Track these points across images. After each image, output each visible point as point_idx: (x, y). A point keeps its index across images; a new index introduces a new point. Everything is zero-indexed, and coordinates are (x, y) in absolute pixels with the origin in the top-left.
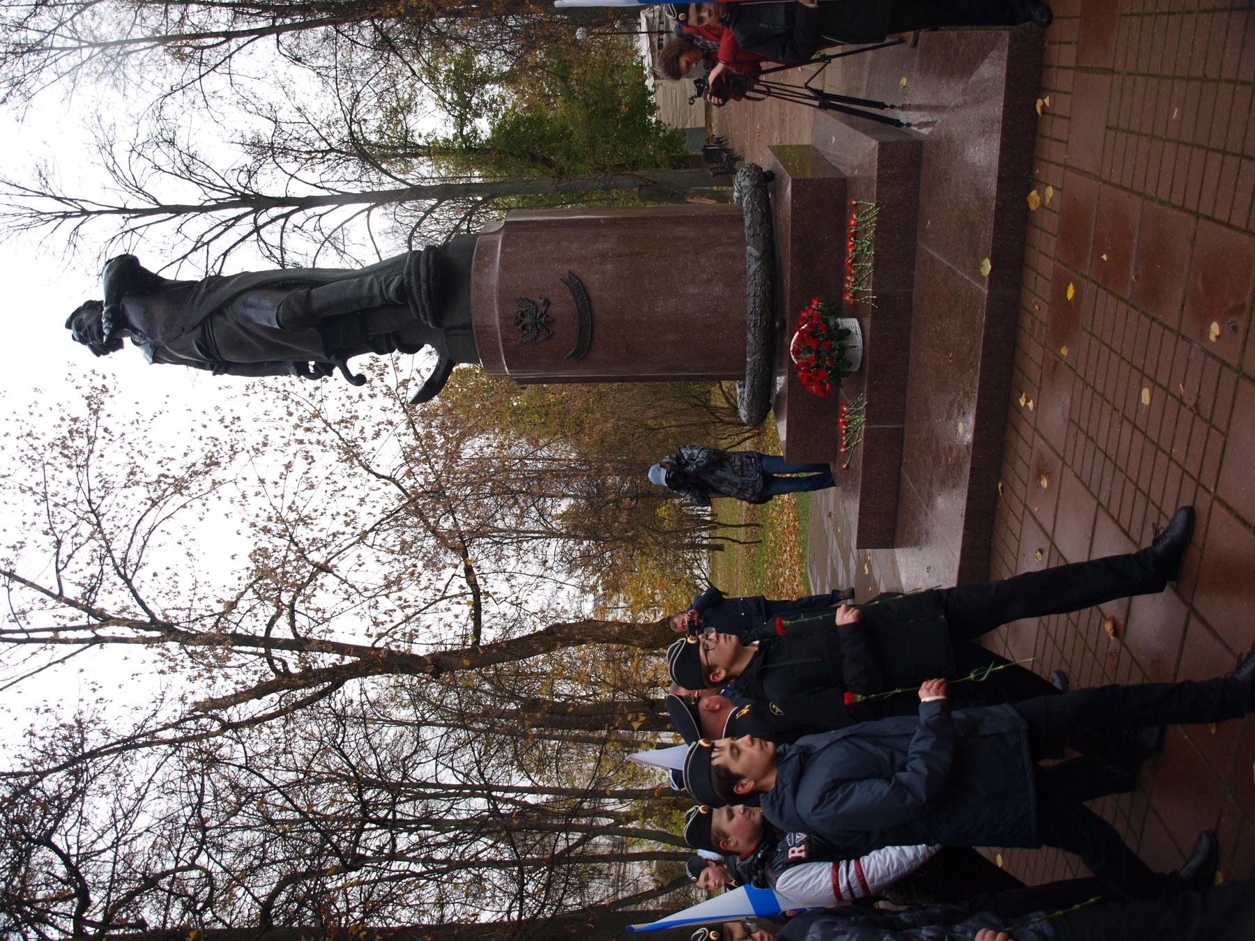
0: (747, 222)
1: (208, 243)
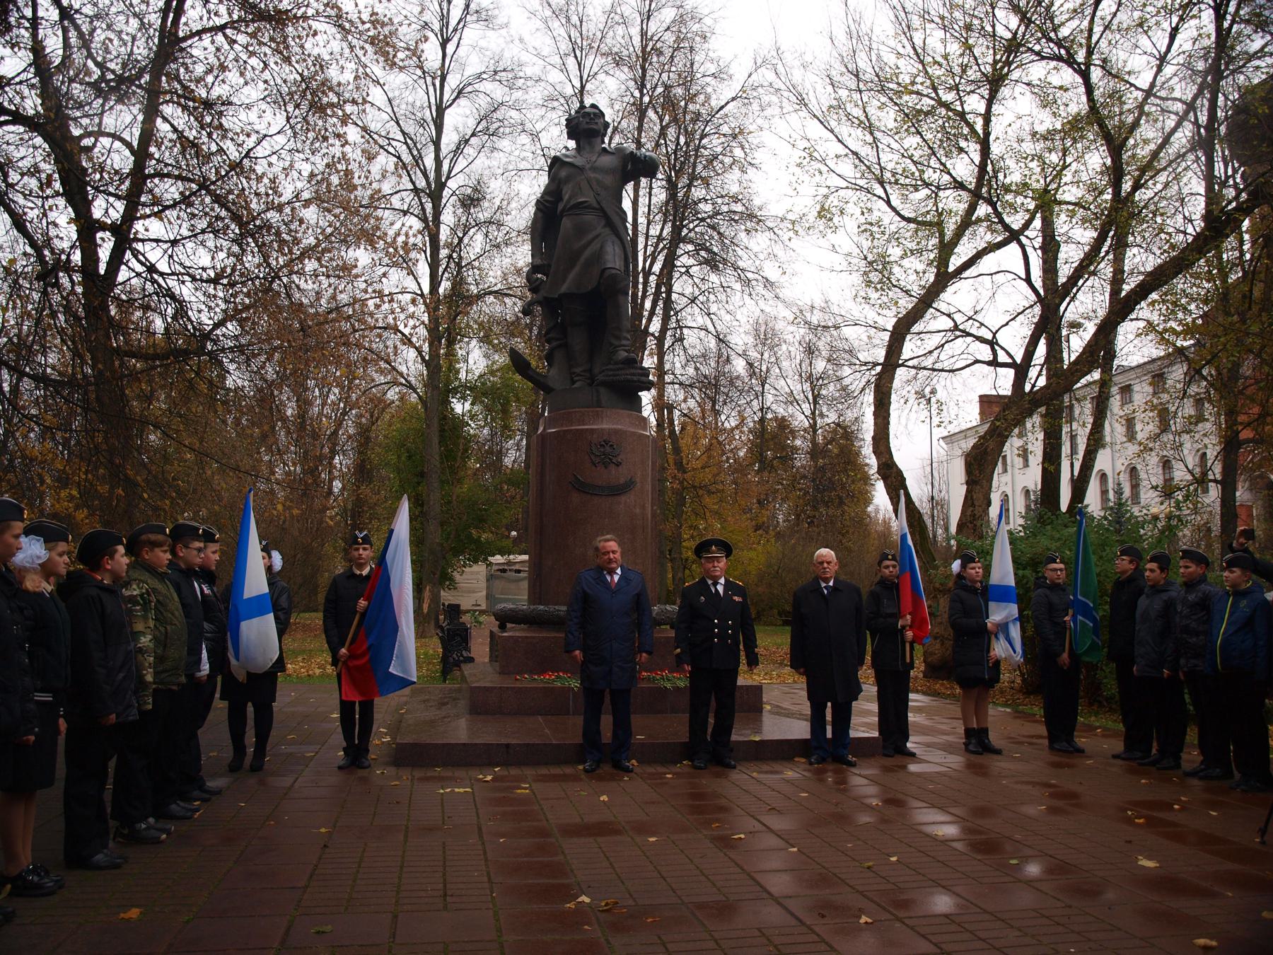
0: (668, 607)
1: (406, 143)
